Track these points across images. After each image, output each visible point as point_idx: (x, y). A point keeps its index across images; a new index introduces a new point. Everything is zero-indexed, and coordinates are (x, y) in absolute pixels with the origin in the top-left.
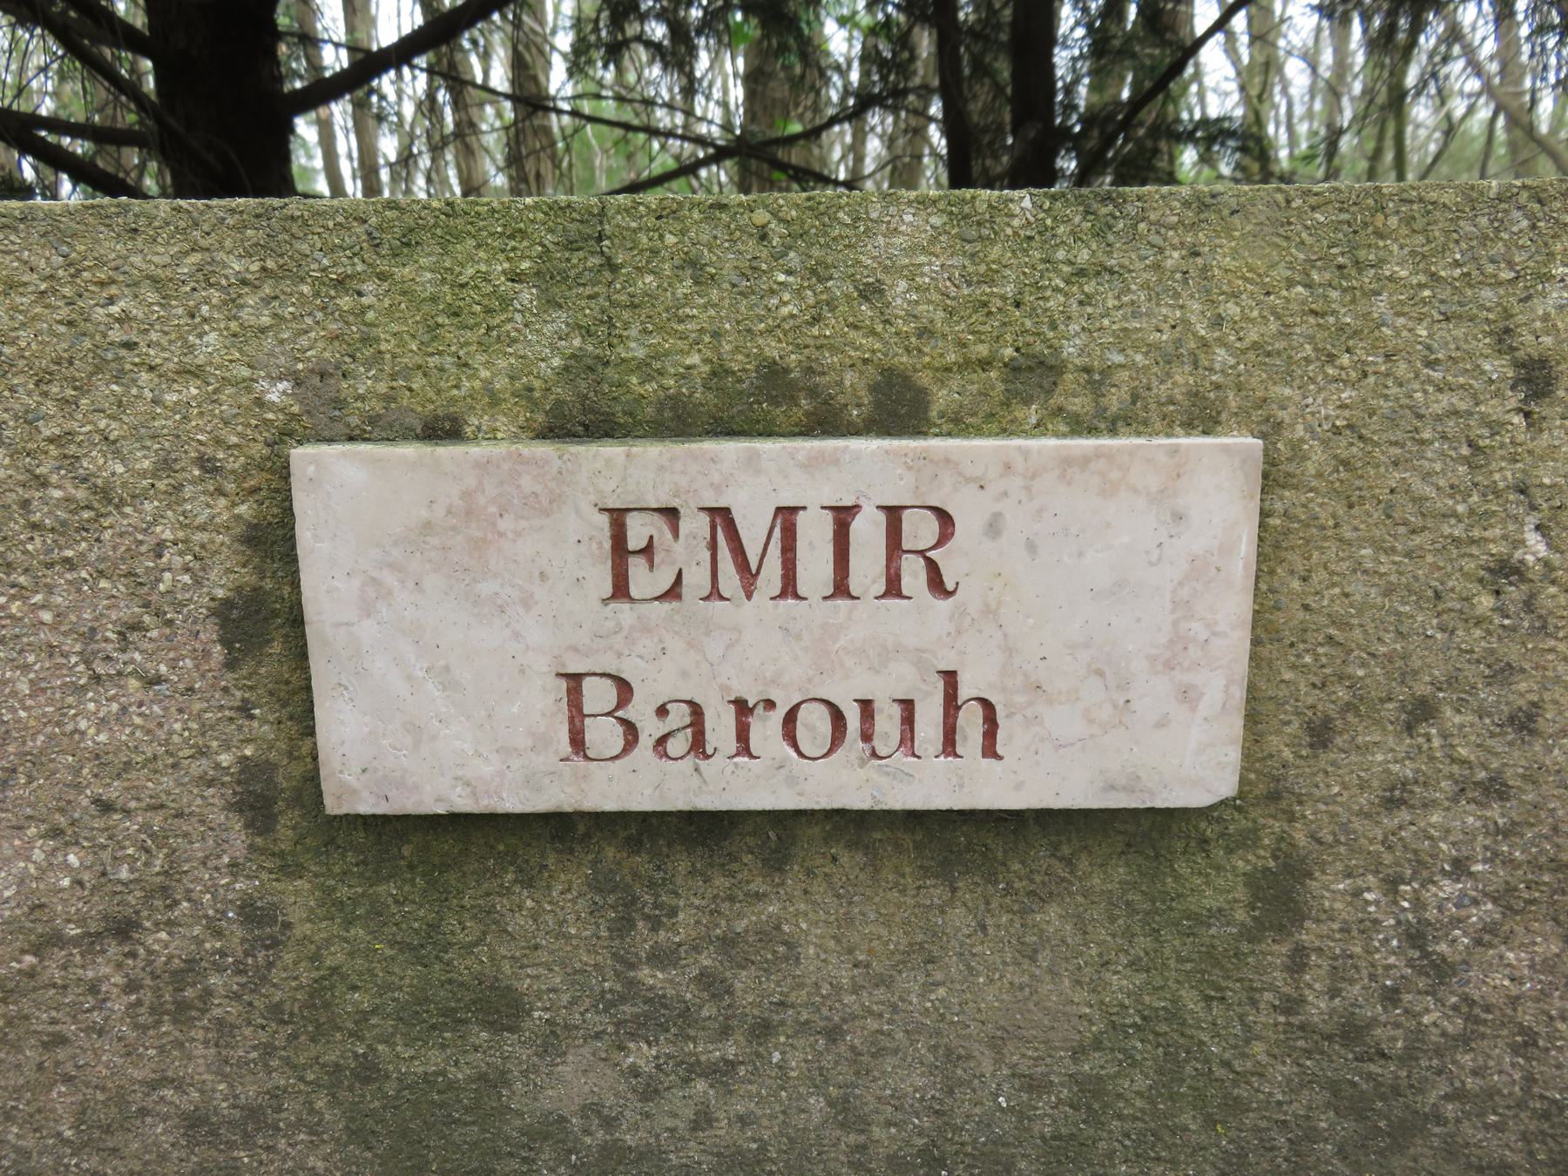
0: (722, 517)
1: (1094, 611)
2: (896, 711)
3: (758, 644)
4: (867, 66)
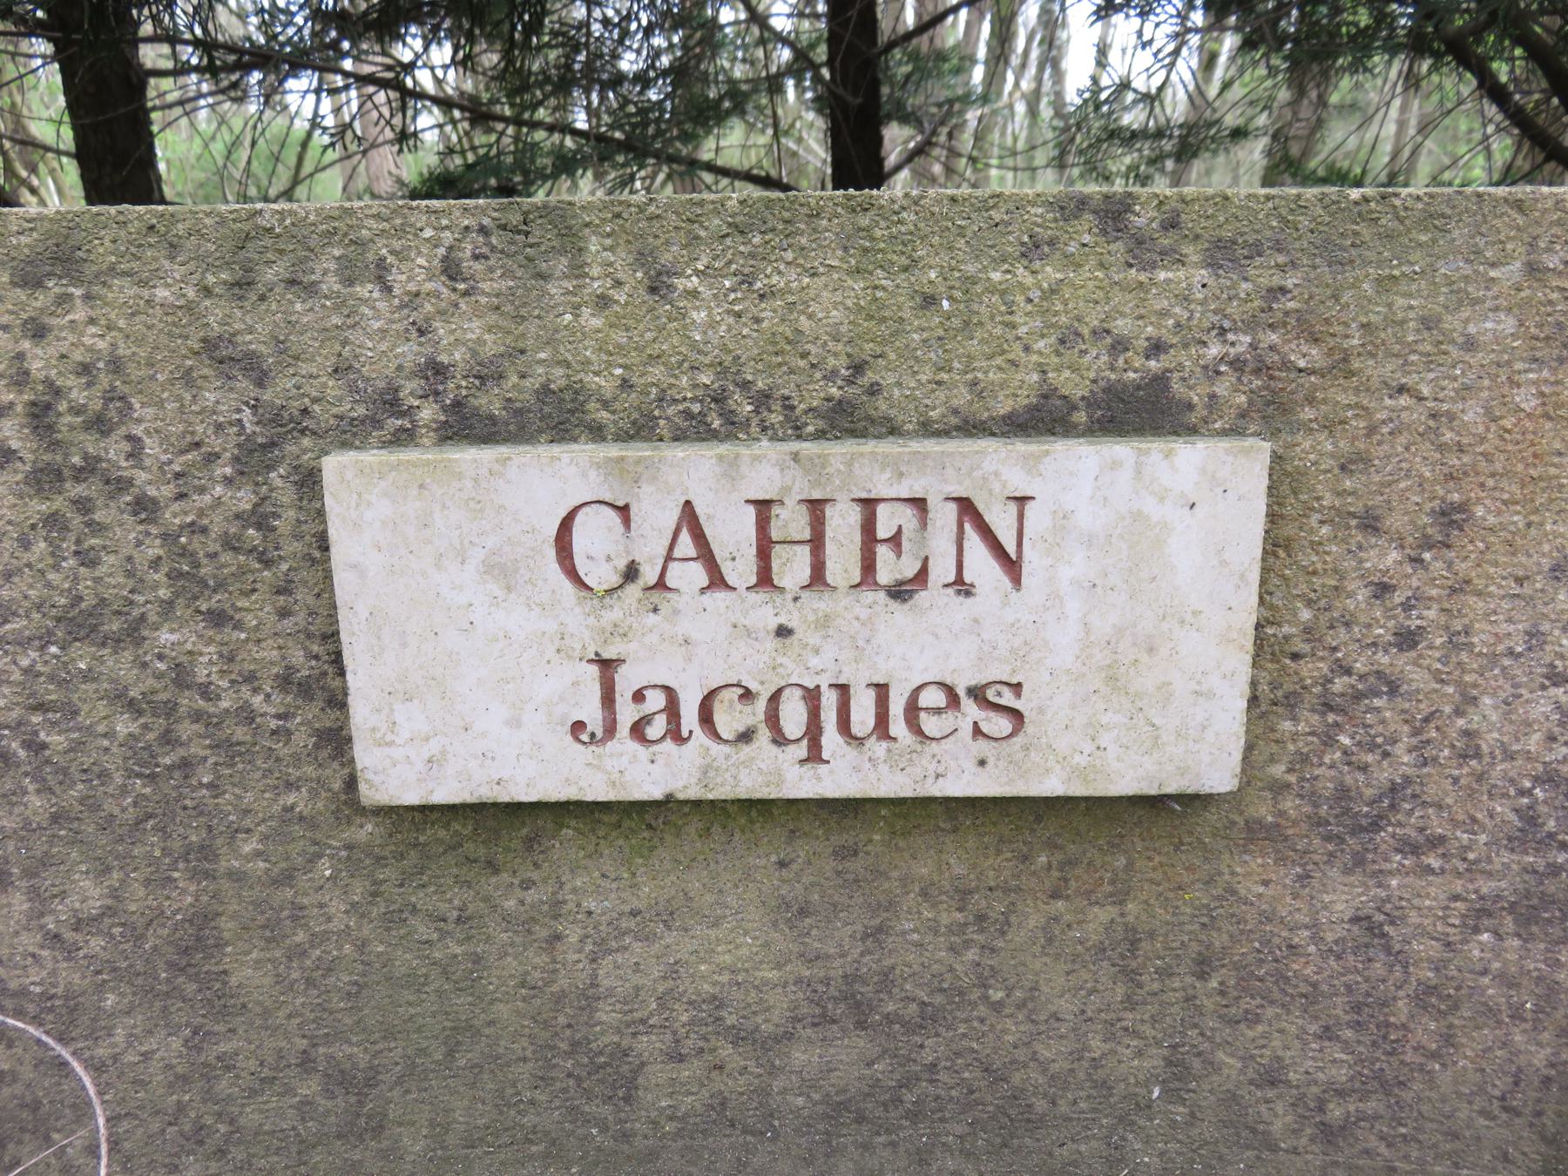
0: (966, 507)
1: (1111, 611)
4: (968, 51)
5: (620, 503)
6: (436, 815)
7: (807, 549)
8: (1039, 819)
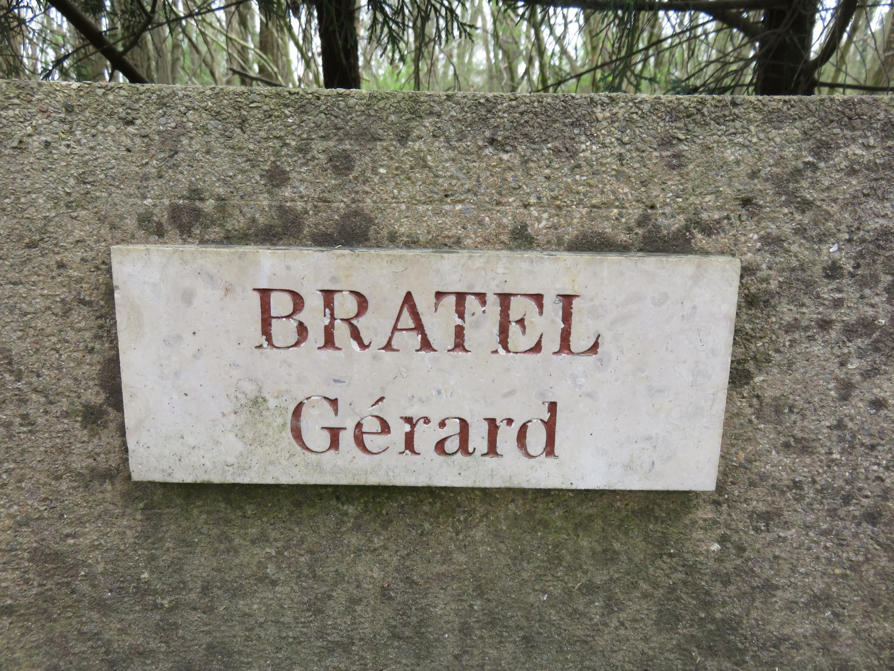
1: (631, 380)
2: (485, 426)
3: (360, 377)
5: (332, 398)
6: (588, 509)
7: (273, 313)
8: (298, 504)
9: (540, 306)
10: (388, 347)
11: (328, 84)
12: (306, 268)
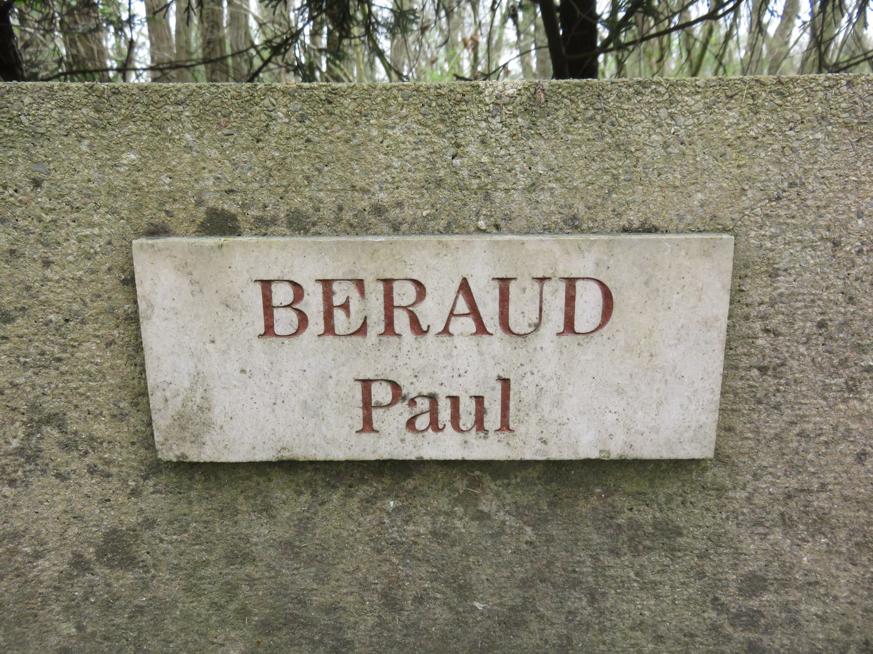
1: (630, 366)
9: (362, 292)
10: (446, 331)
11: (559, 74)
12: (303, 260)
